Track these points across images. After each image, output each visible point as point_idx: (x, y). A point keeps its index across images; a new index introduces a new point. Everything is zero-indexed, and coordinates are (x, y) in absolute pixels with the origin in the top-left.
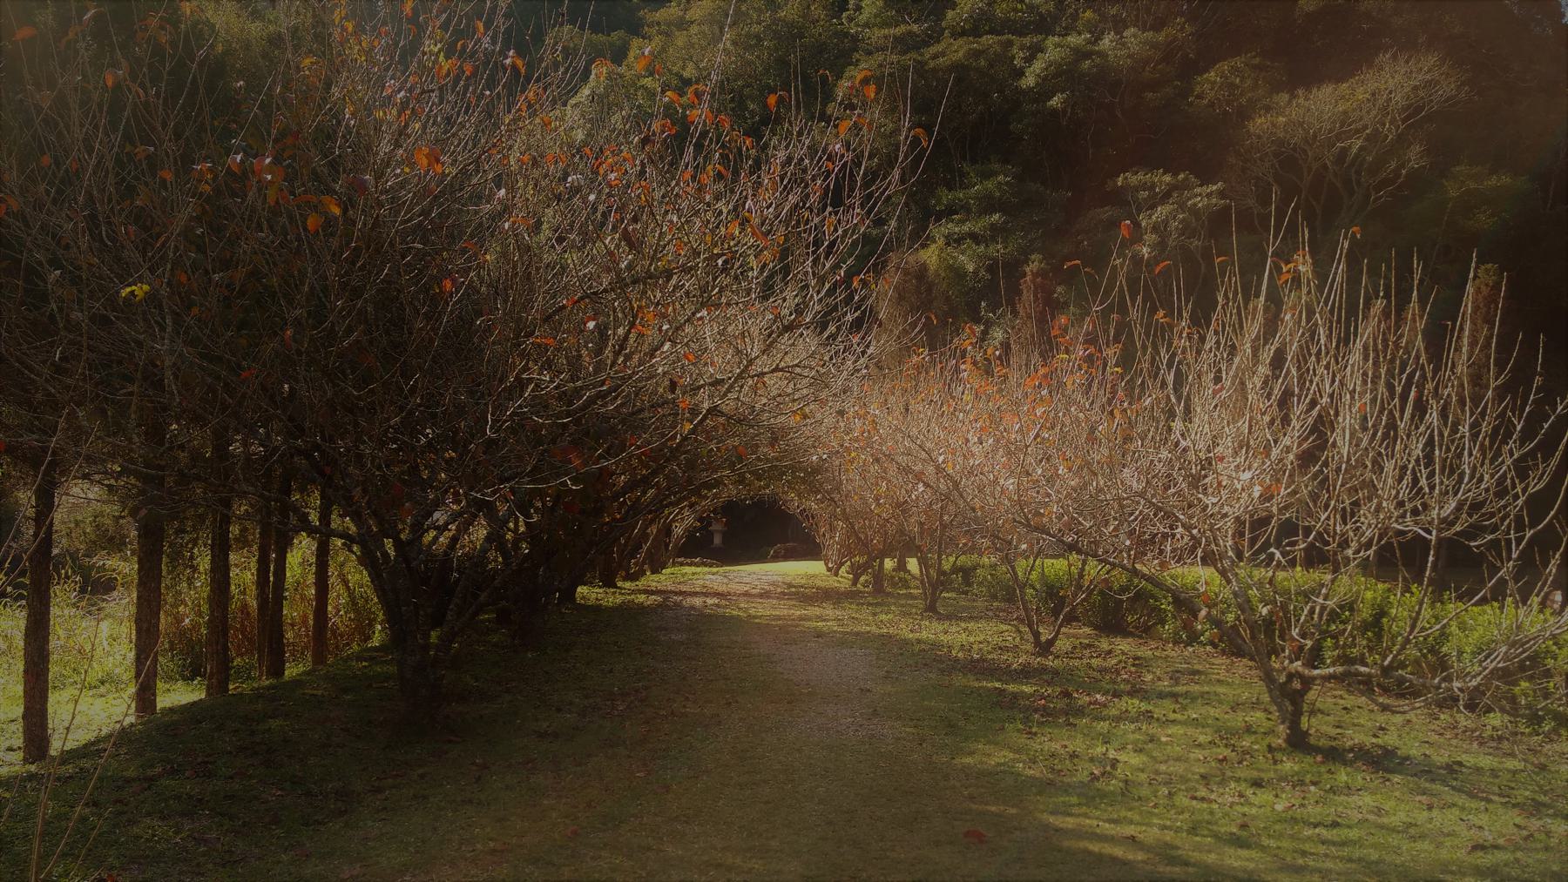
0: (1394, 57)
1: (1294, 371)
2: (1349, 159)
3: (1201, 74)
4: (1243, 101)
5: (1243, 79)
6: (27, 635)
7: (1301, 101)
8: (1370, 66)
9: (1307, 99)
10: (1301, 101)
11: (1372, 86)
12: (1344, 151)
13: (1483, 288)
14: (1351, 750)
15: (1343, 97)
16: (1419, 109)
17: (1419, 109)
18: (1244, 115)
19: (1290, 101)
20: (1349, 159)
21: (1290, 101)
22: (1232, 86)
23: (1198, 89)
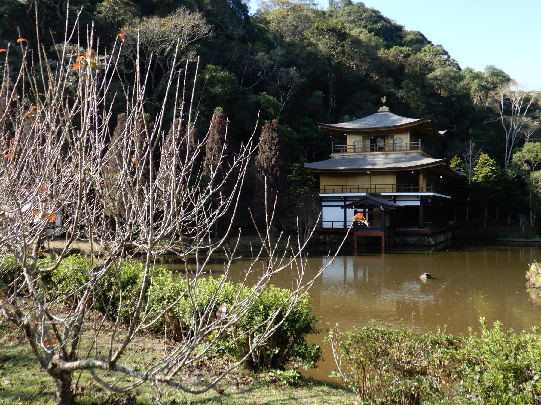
0: (184, 11)
1: (125, 142)
2: (165, 54)
3: (101, 2)
4: (120, 19)
5: (119, 8)
6: (261, 133)
7: (145, 23)
8: (175, 13)
9: (147, 22)
10: (145, 23)
11: (175, 21)
12: (164, 49)
13: (217, 117)
14: (325, 242)
15: (163, 25)
16: (194, 36)
17: (194, 36)
18: (121, 24)
19: (140, 22)
20: (165, 54)
21: (140, 22)
22: (115, 10)
23: (98, 9)
